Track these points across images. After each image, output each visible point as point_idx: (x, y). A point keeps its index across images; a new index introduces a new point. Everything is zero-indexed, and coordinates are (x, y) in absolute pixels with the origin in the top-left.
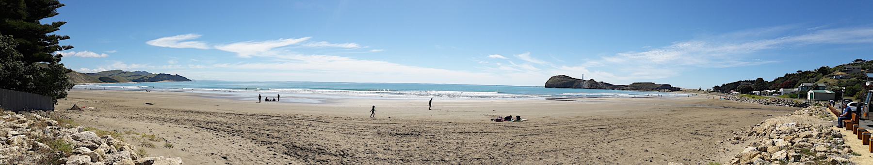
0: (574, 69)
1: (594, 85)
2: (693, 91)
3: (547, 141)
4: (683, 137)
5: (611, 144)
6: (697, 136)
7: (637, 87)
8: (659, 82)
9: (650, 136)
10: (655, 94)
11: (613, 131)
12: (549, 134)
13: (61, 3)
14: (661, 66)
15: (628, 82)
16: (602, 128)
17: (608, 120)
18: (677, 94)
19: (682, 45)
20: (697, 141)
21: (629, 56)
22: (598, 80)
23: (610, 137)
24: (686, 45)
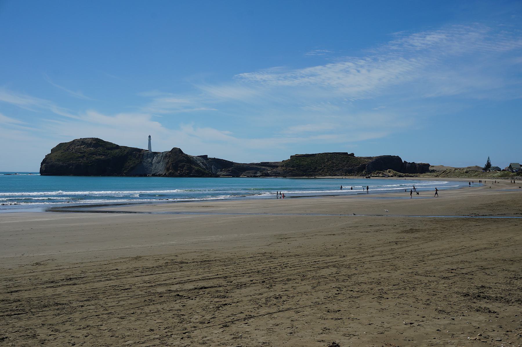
0: (122, 119)
1: (181, 165)
2: (163, 214)
3: (42, 333)
4: (443, 305)
5: (234, 328)
6: (483, 304)
7: (303, 167)
8: (365, 149)
9: (345, 305)
10: (353, 186)
11: (237, 294)
12: (49, 313)
13: (486, 163)
14: (365, 103)
15: (279, 153)
16: (211, 283)
17: (226, 262)
18: (424, 184)
19: (417, 41)
20: (482, 317)
21: (269, 79)
22: (192, 150)
23: (228, 311)
24: (433, 38)
